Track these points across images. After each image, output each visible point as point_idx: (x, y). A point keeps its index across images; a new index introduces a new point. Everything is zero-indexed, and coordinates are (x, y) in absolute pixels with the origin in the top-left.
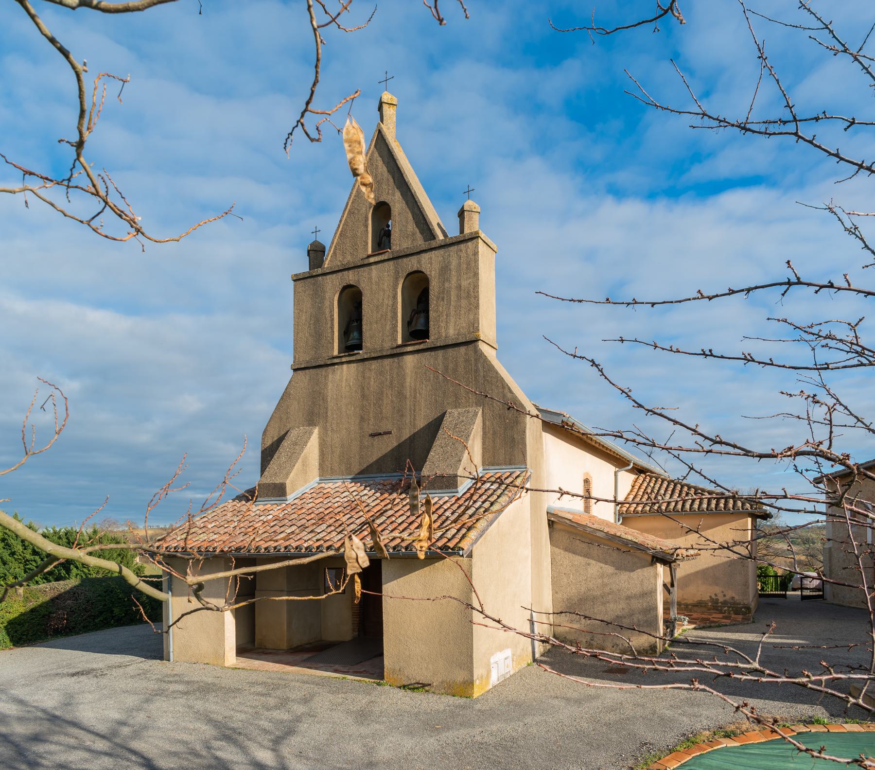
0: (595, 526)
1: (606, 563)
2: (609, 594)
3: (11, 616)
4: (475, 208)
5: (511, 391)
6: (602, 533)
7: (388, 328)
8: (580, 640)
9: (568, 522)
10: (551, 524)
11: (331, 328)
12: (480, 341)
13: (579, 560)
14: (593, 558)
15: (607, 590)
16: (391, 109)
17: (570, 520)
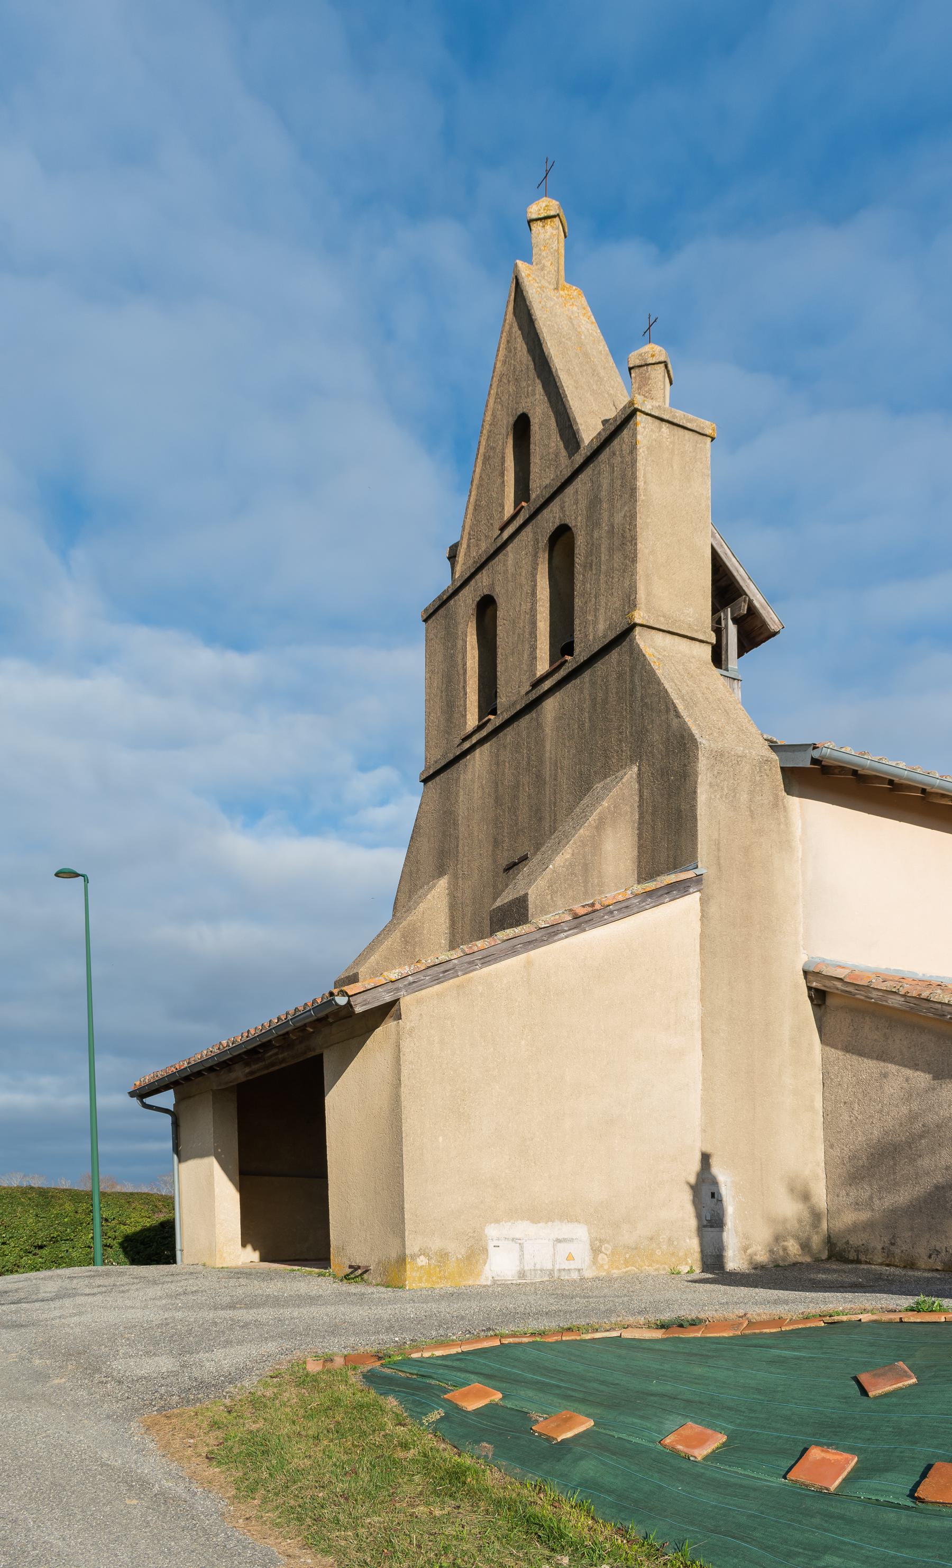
0: (883, 986)
1: (915, 1067)
2: (921, 1137)
3: (129, 1230)
4: (653, 356)
5: (678, 715)
6: (898, 998)
7: (526, 656)
8: (872, 1245)
9: (839, 985)
10: (819, 997)
11: (464, 686)
12: (638, 629)
13: (869, 1067)
14: (892, 1060)
15: (918, 1126)
16: (548, 227)
17: (840, 980)
